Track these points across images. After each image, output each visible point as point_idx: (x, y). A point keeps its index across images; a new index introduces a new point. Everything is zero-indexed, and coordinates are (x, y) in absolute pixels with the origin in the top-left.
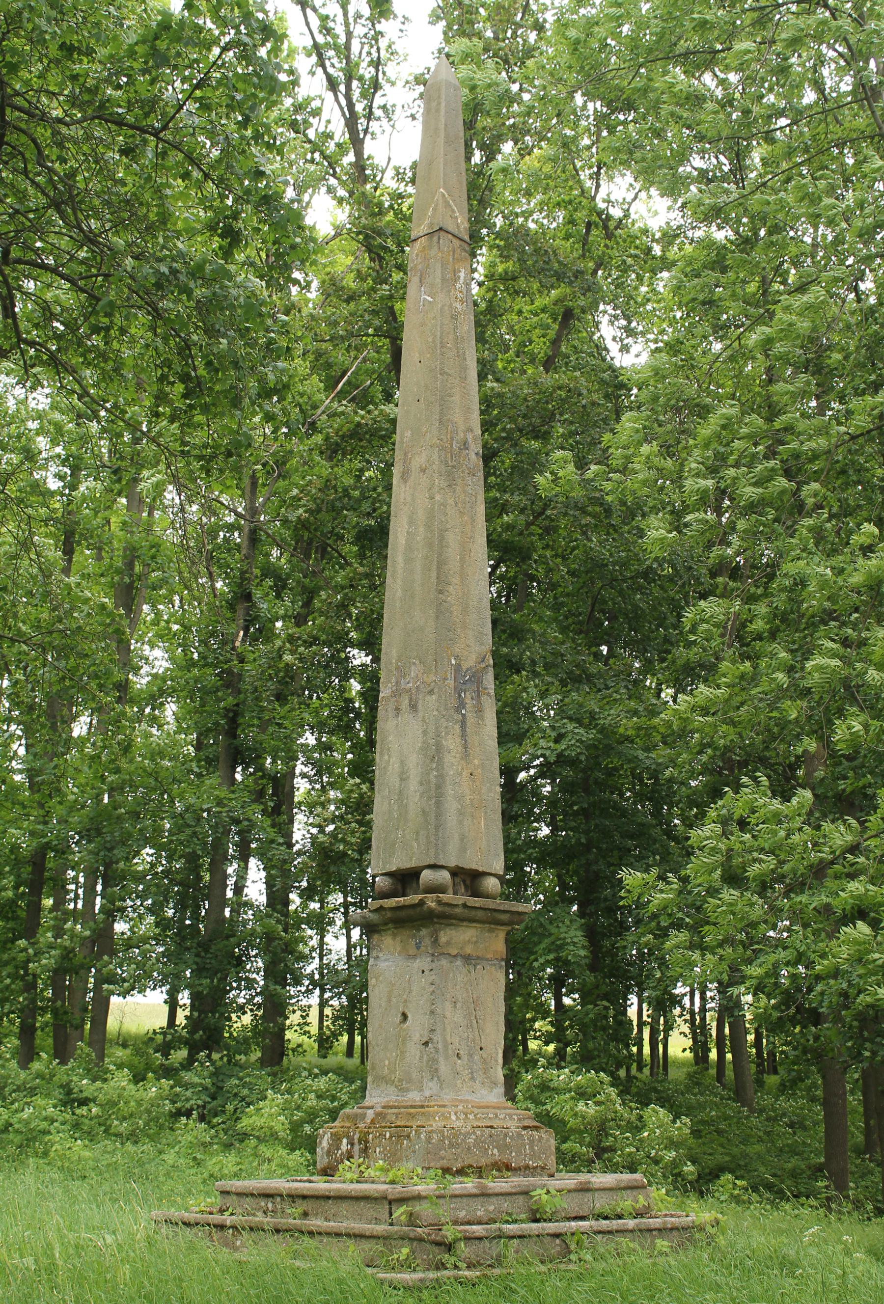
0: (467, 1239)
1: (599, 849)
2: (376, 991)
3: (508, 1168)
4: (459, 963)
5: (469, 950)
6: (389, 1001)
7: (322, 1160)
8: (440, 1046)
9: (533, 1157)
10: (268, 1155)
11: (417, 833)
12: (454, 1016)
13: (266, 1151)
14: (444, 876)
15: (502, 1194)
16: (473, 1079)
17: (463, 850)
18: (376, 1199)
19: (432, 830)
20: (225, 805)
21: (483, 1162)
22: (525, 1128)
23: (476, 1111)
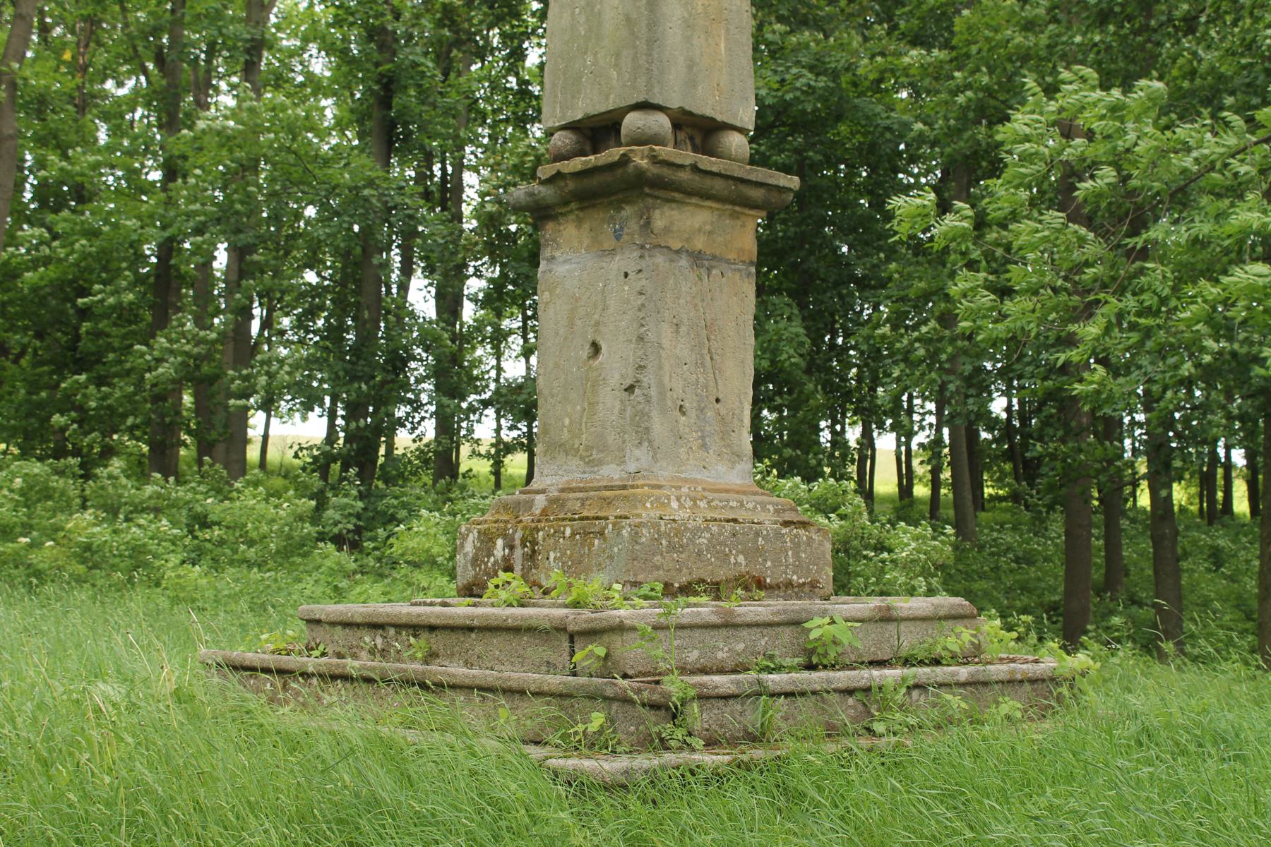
0: (703, 698)
1: (811, 243)
2: (551, 312)
3: (761, 584)
4: (684, 262)
5: (699, 243)
6: (571, 325)
7: (466, 574)
8: (653, 392)
9: (797, 568)
10: (424, 584)
11: (618, 55)
12: (675, 348)
13: (421, 577)
14: (661, 123)
15: (757, 625)
16: (704, 446)
17: (691, 84)
18: (546, 632)
19: (642, 46)
20: (378, 187)
21: (722, 574)
22: (786, 524)
23: (710, 496)
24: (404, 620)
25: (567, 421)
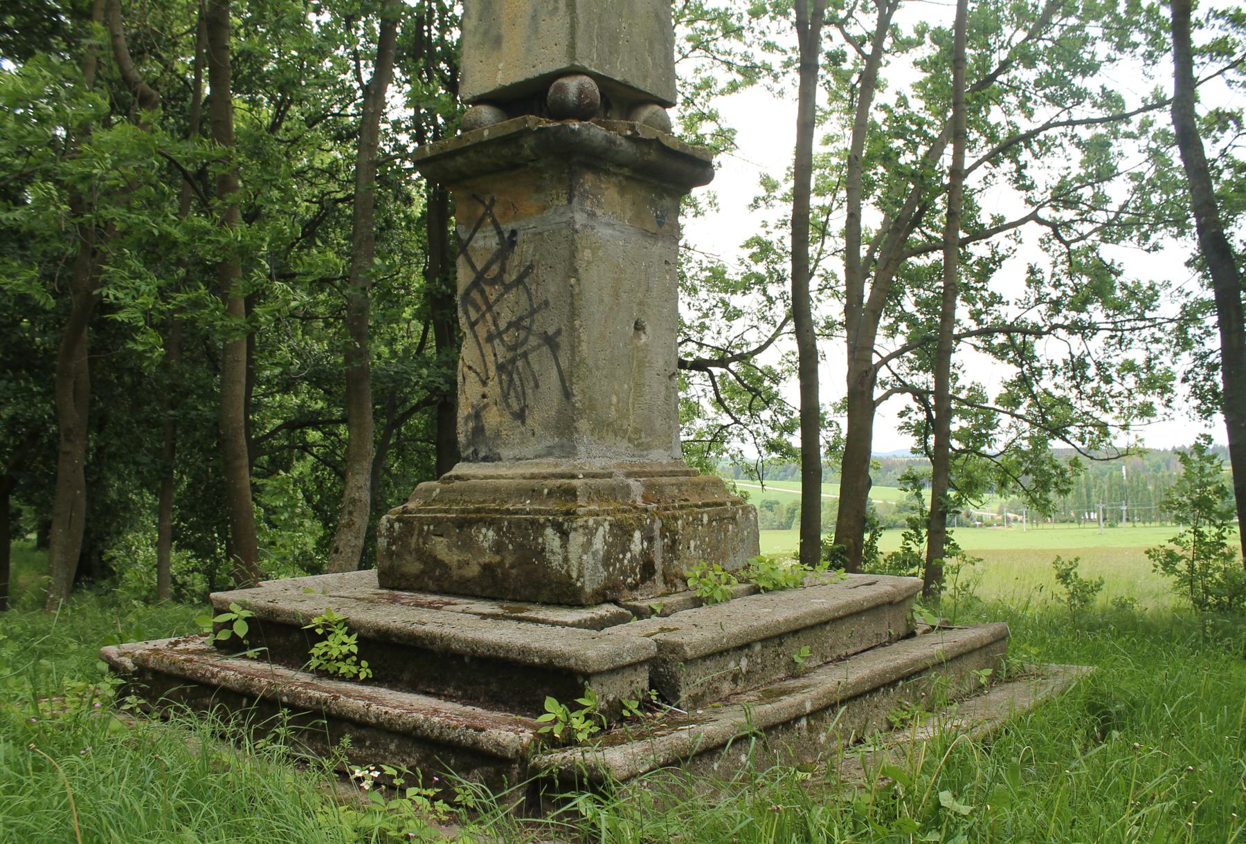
24: (783, 629)
25: (614, 399)
